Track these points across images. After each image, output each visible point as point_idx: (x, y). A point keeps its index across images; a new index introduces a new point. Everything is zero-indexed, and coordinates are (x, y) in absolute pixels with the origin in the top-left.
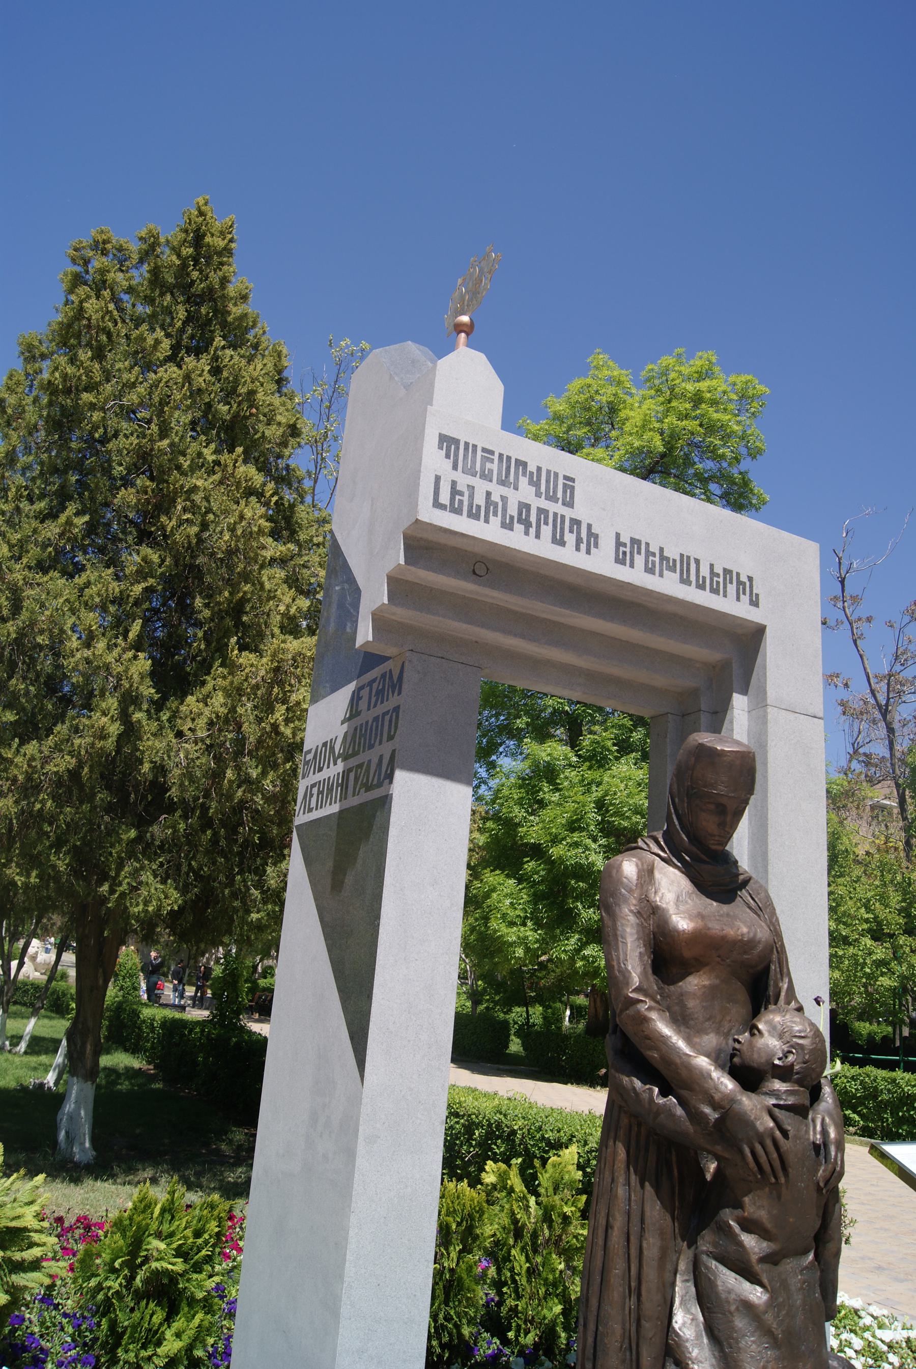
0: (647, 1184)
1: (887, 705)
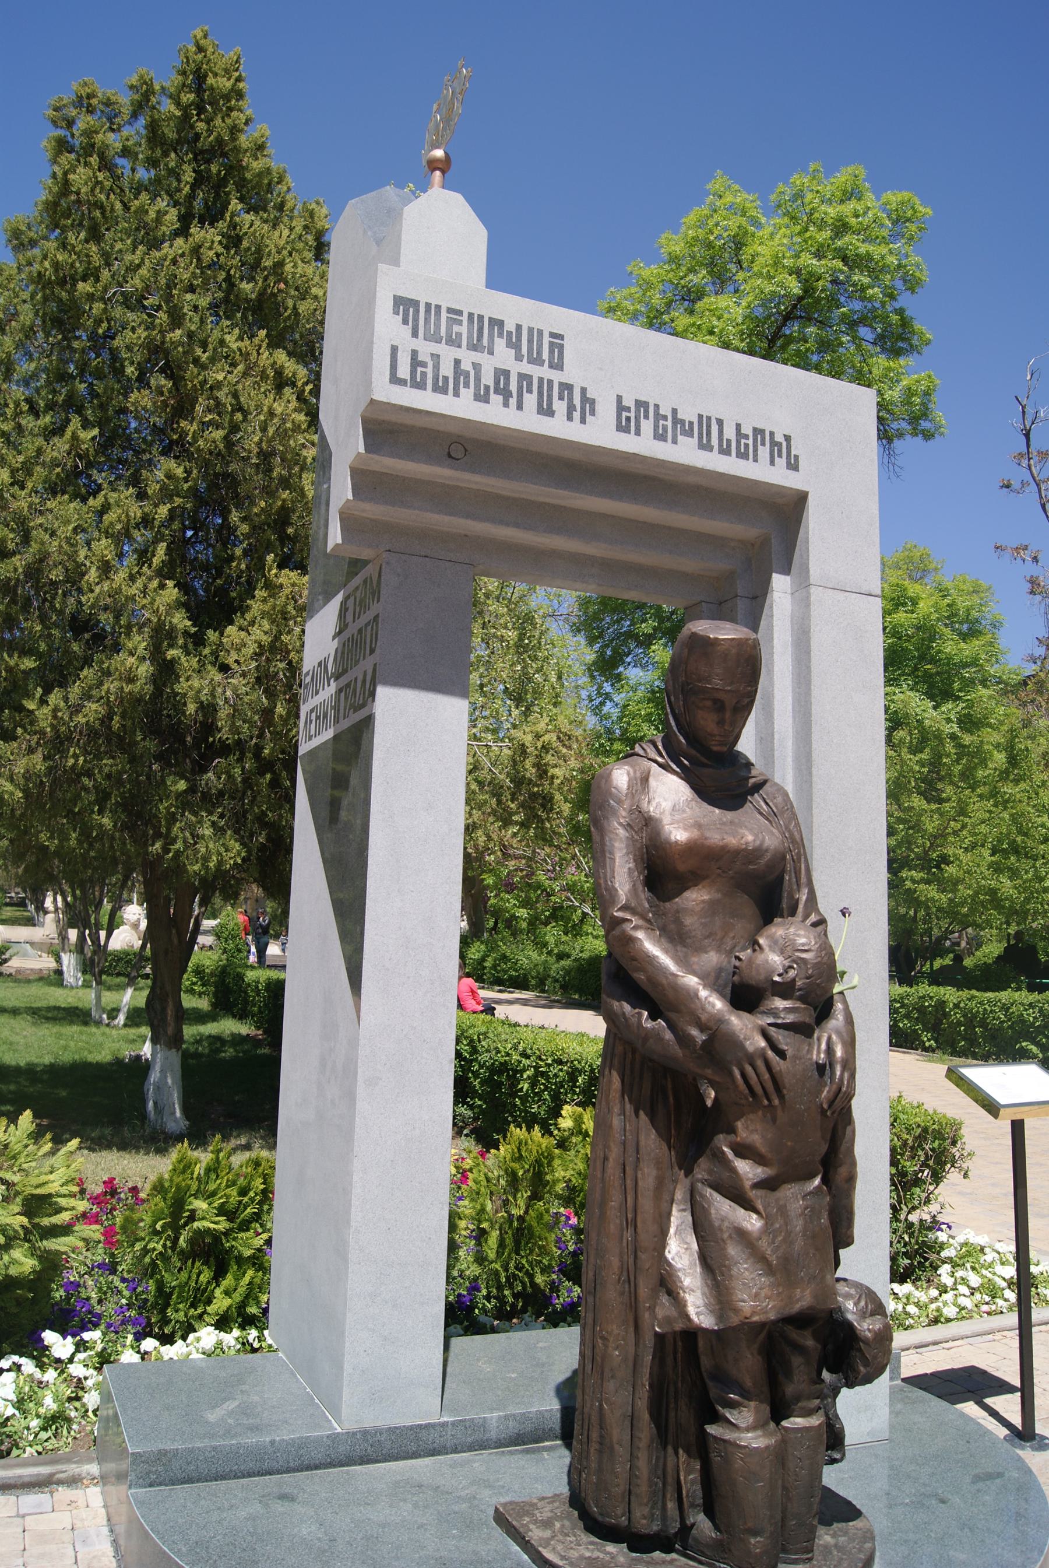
0: (641, 1113)
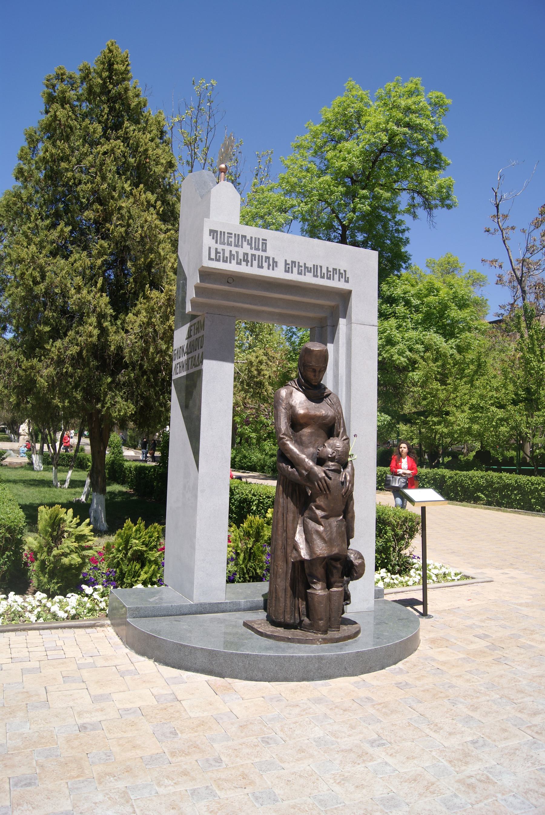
1: (522, 277)
